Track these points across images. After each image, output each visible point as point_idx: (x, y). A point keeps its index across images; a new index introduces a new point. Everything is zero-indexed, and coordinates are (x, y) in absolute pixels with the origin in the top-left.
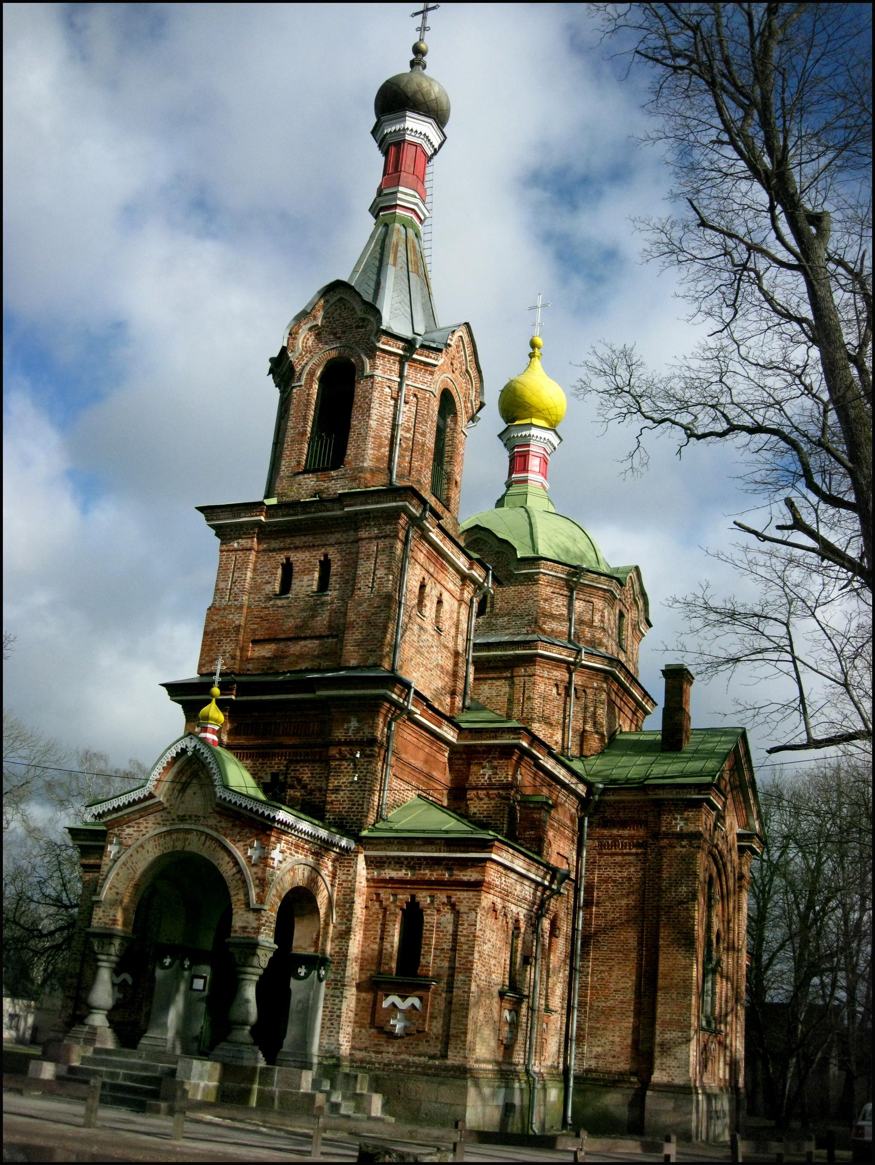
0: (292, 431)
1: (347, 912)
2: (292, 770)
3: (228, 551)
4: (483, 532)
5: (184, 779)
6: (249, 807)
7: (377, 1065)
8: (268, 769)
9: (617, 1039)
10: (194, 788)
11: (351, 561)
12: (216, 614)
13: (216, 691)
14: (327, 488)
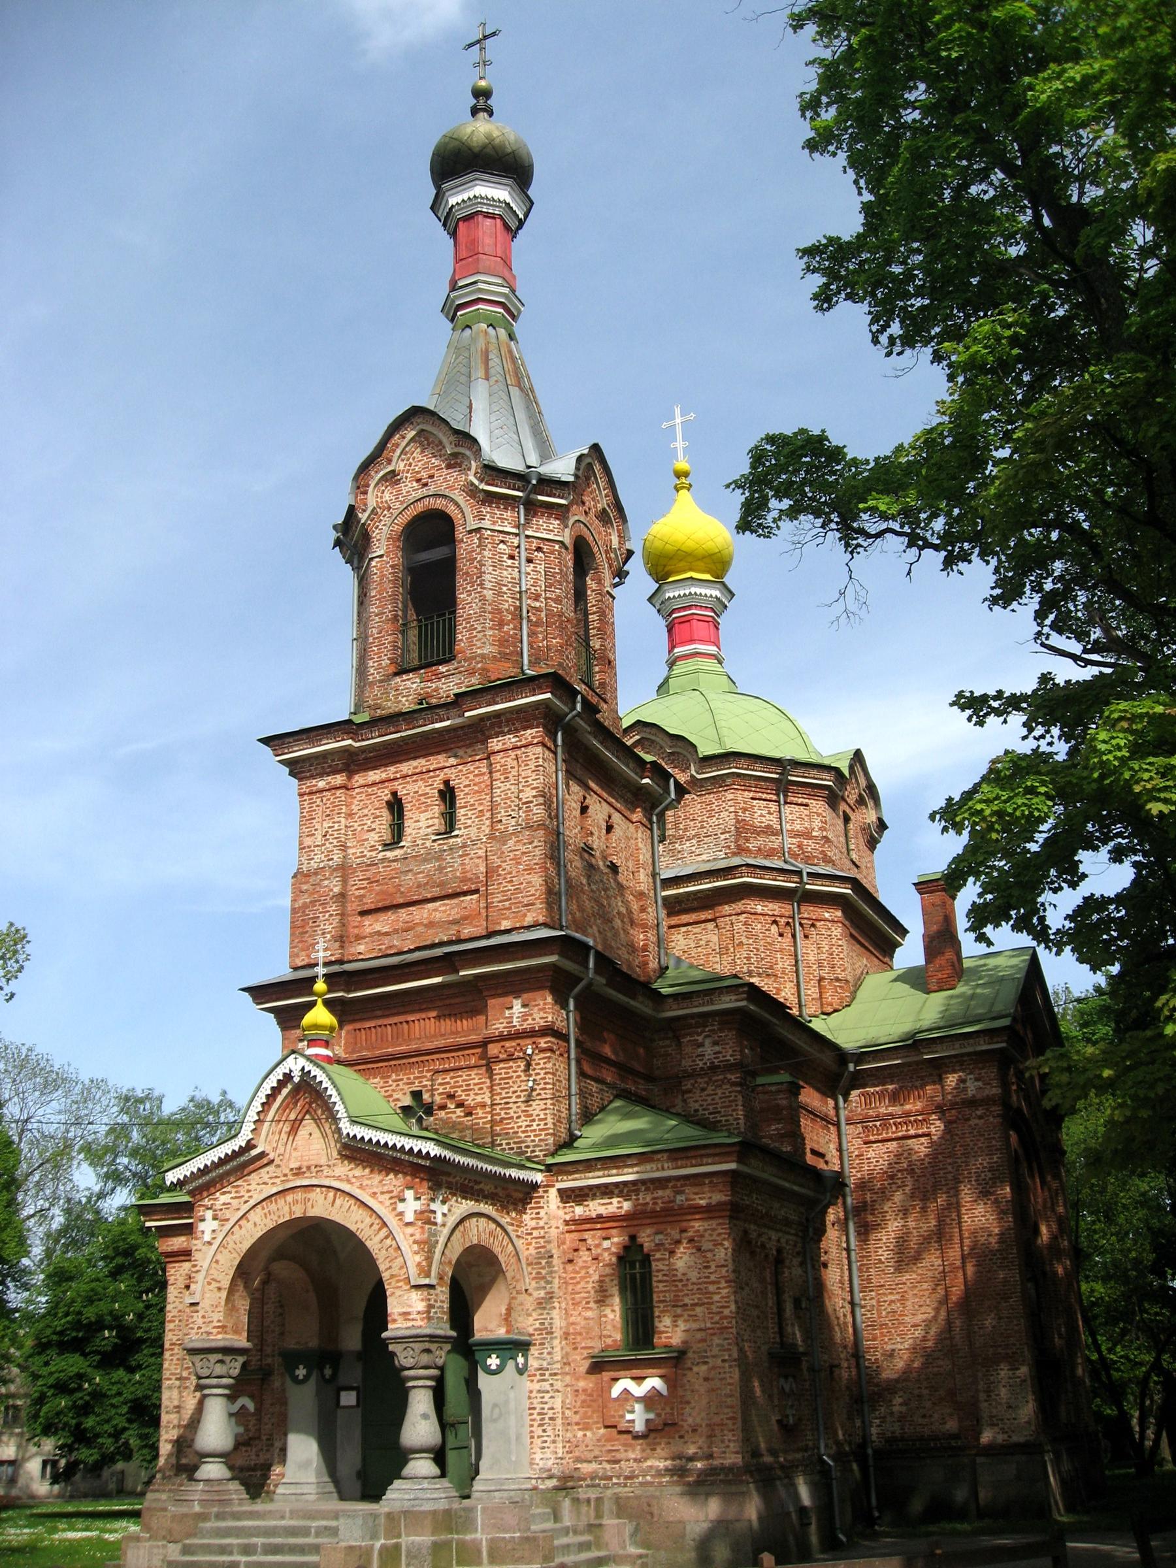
0: (377, 619)
1: (543, 1272)
2: (440, 1084)
3: (311, 793)
4: (648, 730)
5: (292, 1116)
6: (416, 1150)
7: (615, 1480)
8: (406, 1087)
9: (925, 1392)
10: (309, 1125)
11: (483, 785)
12: (304, 883)
13: (320, 986)
14: (436, 690)
